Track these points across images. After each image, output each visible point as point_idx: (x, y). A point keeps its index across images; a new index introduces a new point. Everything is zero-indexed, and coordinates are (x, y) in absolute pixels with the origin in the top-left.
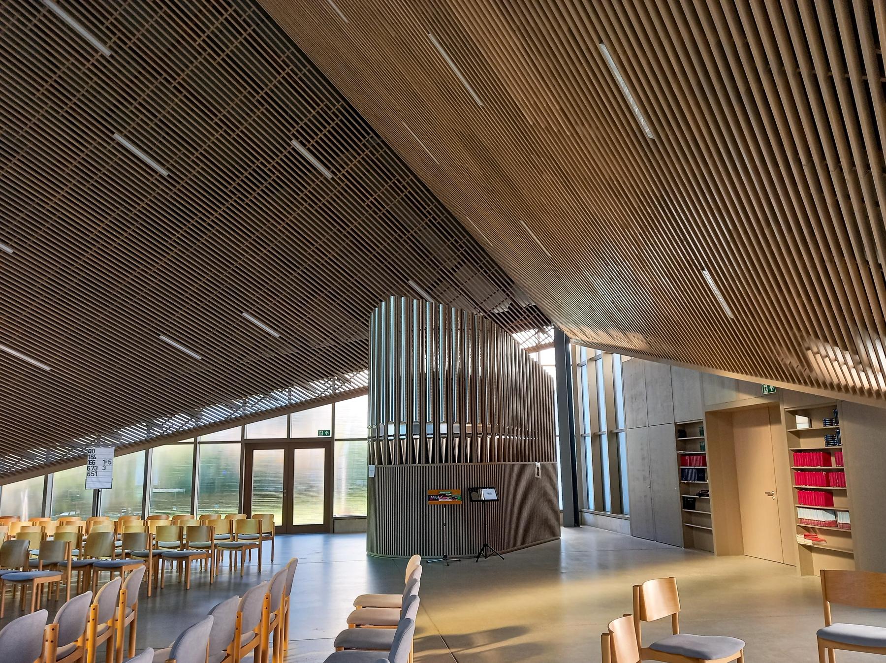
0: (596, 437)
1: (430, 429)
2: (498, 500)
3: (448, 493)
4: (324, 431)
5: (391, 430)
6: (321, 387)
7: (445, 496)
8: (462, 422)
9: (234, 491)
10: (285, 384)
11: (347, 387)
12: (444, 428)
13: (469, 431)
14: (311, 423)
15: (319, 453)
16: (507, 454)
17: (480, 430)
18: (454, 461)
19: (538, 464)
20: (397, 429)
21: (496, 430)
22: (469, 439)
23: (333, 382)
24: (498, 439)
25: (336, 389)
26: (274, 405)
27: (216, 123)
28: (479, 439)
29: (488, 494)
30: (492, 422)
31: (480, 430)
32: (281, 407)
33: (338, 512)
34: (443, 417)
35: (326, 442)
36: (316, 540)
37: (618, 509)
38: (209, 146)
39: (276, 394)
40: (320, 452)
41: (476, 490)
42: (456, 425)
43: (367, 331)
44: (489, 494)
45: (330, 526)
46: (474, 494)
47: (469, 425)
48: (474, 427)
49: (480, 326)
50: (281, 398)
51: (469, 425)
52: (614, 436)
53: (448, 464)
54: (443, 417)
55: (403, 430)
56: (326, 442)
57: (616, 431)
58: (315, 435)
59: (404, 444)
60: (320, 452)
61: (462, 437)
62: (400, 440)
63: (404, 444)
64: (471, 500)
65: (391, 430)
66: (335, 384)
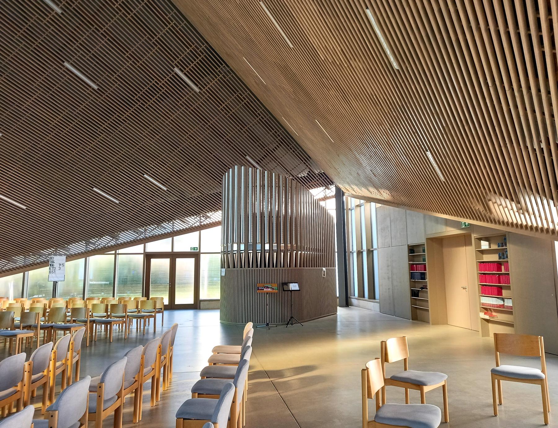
0: (360, 253)
1: (259, 247)
2: (299, 290)
3: (269, 286)
4: (194, 248)
5: (235, 247)
6: (193, 221)
7: (268, 287)
8: (278, 243)
9: (139, 284)
10: (170, 219)
11: (208, 221)
12: (267, 247)
13: (282, 248)
14: (184, 243)
15: (191, 261)
16: (305, 262)
17: (289, 247)
18: (273, 267)
19: (324, 269)
20: (239, 247)
21: (299, 248)
22: (282, 254)
23: (200, 217)
24: (300, 254)
25: (201, 222)
26: (163, 231)
27: (131, 60)
28: (289, 253)
29: (294, 287)
30: (296, 243)
31: (289, 247)
32: (168, 233)
33: (202, 297)
34: (267, 240)
35: (195, 255)
36: (189, 314)
37: (372, 296)
38: (123, 71)
39: (165, 225)
40: (193, 260)
41: (286, 284)
42: (275, 245)
43: (221, 187)
44: (295, 286)
45: (197, 305)
46: (285, 286)
47: (282, 245)
48: (286, 246)
49: (290, 185)
50: (168, 227)
51: (282, 245)
52: (370, 252)
53: (253, 269)
54: (267, 240)
55: (242, 247)
56: (195, 255)
57: (372, 249)
58: (189, 250)
59: (243, 256)
60: (193, 260)
61: (278, 251)
62: (240, 253)
63: (243, 256)
64: (284, 290)
65: (235, 247)
66: (201, 219)
